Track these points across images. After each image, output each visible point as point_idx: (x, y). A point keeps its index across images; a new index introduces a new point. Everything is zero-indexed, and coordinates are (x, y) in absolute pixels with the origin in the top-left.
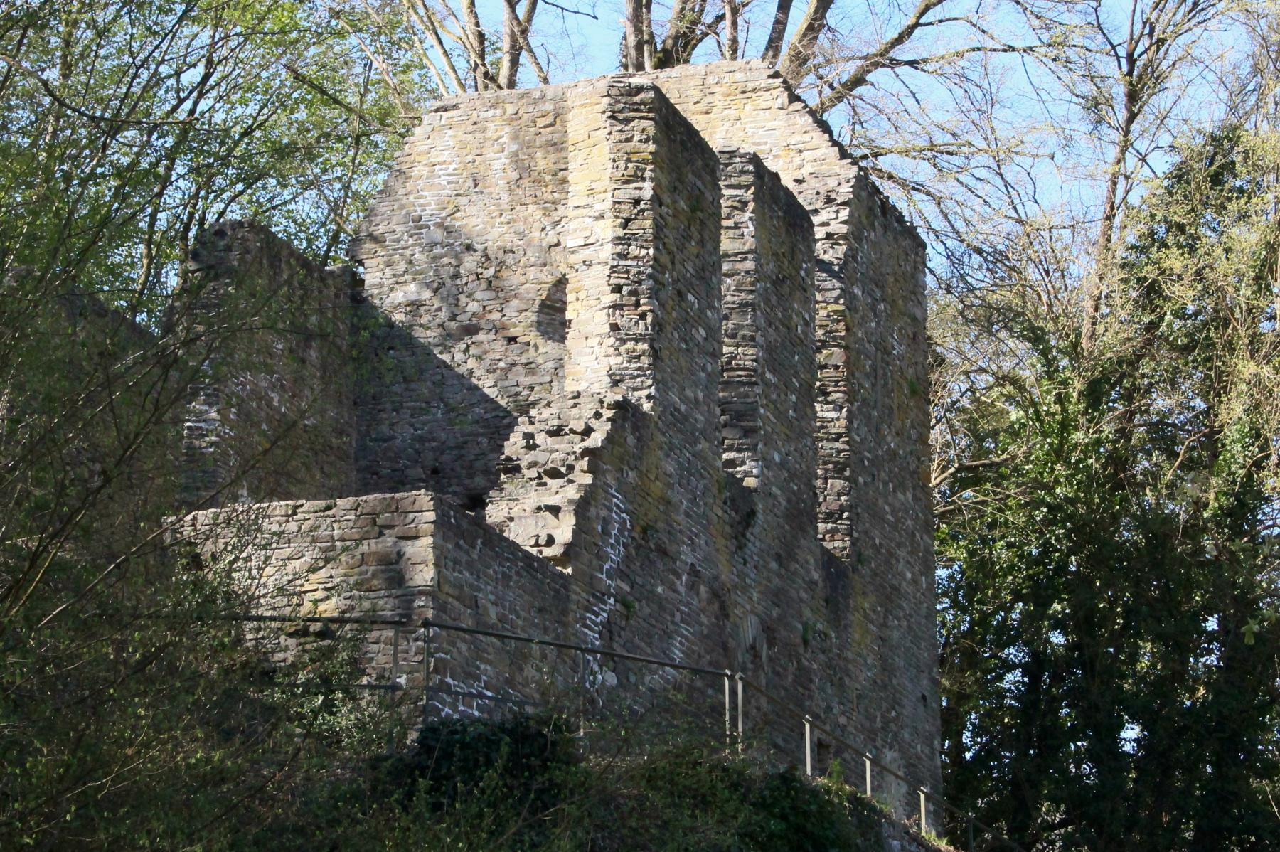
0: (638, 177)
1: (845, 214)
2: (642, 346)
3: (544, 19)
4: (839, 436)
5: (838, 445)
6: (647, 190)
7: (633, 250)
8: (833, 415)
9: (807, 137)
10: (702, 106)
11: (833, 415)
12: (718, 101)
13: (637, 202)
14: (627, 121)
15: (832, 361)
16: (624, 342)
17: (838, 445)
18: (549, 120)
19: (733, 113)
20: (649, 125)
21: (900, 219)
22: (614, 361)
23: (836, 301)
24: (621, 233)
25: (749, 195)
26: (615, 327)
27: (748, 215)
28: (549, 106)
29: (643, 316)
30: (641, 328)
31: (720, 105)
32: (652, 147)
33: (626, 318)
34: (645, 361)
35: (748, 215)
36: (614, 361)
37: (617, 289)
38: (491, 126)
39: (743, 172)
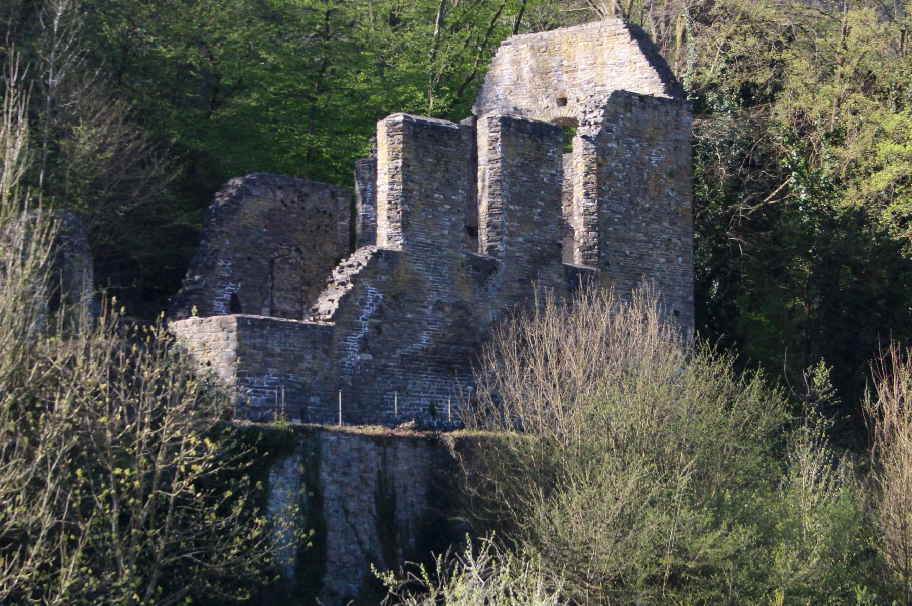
0: (397, 158)
1: (602, 112)
2: (399, 224)
3: (528, 4)
4: (594, 213)
5: (593, 217)
6: (400, 163)
7: (395, 186)
8: (591, 204)
9: (637, 57)
10: (599, 42)
11: (591, 204)
12: (605, 40)
13: (396, 168)
14: (392, 136)
15: (591, 180)
16: (392, 223)
17: (593, 217)
18: (544, 49)
19: (610, 45)
20: (400, 137)
21: (475, 170)
22: (389, 230)
23: (593, 154)
24: (391, 180)
25: (499, 135)
26: (389, 217)
27: (499, 143)
28: (544, 43)
29: (398, 213)
30: (398, 218)
31: (606, 41)
32: (401, 146)
33: (393, 213)
34: (400, 230)
35: (499, 143)
36: (389, 230)
37: (389, 202)
38: (523, 52)
39: (497, 126)
